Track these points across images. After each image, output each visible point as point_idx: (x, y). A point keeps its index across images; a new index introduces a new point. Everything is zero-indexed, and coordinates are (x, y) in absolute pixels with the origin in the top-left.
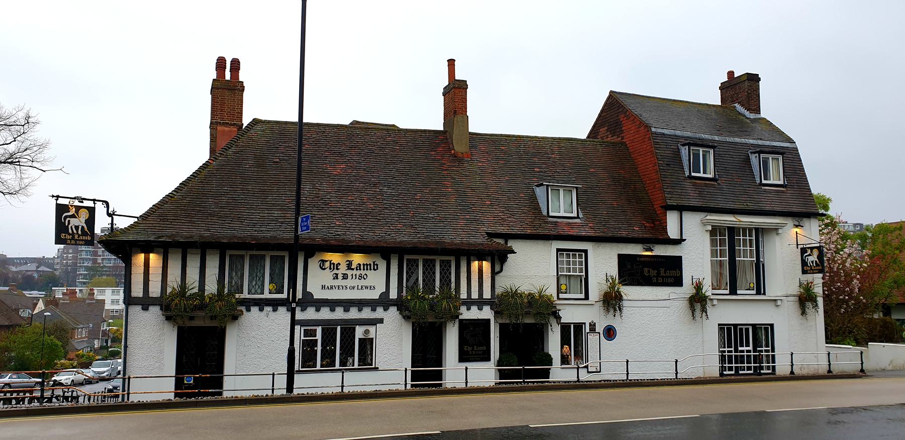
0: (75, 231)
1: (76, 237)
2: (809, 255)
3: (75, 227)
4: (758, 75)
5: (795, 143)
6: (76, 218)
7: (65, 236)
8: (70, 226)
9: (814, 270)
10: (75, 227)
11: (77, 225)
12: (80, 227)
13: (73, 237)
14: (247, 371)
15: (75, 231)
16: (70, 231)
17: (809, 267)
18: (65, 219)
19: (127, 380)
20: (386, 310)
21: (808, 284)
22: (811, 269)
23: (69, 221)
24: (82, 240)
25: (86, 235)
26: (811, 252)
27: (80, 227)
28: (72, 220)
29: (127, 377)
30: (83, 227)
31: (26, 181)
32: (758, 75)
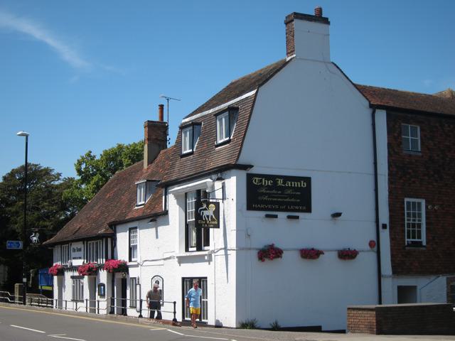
1: (208, 222)
2: (205, 209)
26: (208, 206)
28: (205, 212)
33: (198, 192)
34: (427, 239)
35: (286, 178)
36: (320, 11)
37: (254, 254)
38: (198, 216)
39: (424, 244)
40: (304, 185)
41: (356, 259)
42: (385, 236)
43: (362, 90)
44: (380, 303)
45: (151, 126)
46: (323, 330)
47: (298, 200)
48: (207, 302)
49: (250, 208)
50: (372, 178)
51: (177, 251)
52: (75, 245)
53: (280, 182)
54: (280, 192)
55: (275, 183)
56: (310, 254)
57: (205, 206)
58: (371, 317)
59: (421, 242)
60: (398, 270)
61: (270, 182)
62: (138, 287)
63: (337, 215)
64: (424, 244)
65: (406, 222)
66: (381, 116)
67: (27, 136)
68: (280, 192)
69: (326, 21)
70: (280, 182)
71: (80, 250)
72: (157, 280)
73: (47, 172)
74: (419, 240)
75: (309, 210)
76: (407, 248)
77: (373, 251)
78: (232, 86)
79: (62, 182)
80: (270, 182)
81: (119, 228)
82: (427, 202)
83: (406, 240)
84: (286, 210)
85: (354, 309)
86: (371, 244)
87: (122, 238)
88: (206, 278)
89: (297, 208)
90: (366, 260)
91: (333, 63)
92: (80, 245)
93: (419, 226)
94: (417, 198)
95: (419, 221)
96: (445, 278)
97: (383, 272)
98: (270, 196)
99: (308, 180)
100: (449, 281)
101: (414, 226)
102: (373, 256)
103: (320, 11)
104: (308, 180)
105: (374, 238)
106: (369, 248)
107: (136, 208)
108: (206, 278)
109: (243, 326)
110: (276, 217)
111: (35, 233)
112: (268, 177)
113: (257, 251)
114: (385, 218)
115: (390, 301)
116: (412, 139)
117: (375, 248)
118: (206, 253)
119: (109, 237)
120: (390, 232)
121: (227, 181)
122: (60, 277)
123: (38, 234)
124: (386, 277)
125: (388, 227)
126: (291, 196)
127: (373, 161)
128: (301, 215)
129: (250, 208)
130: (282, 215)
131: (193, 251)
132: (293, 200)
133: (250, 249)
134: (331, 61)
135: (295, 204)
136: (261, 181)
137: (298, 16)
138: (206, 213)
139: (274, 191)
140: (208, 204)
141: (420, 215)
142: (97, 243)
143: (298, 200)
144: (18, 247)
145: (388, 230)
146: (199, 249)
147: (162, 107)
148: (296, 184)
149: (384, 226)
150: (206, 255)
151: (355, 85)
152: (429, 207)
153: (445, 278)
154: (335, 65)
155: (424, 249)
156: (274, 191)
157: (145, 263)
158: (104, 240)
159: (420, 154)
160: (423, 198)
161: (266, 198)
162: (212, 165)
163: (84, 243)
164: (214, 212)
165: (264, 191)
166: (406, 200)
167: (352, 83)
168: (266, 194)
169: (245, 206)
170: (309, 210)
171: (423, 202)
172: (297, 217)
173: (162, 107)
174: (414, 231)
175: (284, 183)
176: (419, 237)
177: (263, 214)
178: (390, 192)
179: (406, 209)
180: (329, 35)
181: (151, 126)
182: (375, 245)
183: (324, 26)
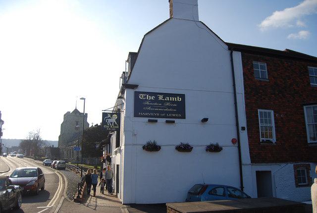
2: (110, 118)
13: (110, 127)
26: (111, 116)
28: (109, 120)
35: (165, 95)
55: (157, 98)
67: (84, 99)
82: (274, 112)
90: (230, 152)
99: (183, 96)
100: (295, 167)
117: (237, 145)
126: (169, 107)
128: (176, 120)
136: (146, 96)
139: (156, 104)
160: (272, 110)
177: (147, 119)
182: (236, 141)
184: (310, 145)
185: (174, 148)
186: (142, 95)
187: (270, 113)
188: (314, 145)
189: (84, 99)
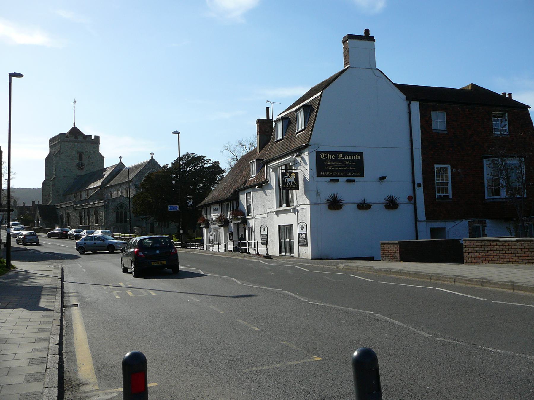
0: (290, 184)
1: (290, 186)
2: (189, 202)
3: (290, 182)
4: (373, 37)
5: (374, 40)
6: (290, 178)
7: (285, 186)
8: (287, 182)
9: (291, 187)
10: (290, 182)
11: (290, 181)
12: (292, 182)
14: (35, 269)
15: (290, 184)
16: (288, 184)
17: (287, 185)
18: (285, 179)
19: (256, 243)
20: (505, 197)
21: (334, 196)
22: (289, 187)
23: (287, 180)
24: (293, 187)
25: (295, 185)
26: (290, 175)
27: (292, 182)
28: (288, 179)
29: (256, 242)
30: (293, 182)
31: (229, 161)
32: (373, 37)
33: (286, 165)
34: (452, 194)
35: (345, 153)
36: (367, 31)
37: (325, 207)
38: (284, 182)
39: (451, 197)
40: (358, 157)
41: (358, 210)
42: (420, 193)
43: (402, 88)
44: (417, 239)
45: (260, 122)
46: (374, 259)
47: (354, 169)
48: (293, 241)
49: (319, 175)
50: (408, 151)
51: (275, 207)
52: (215, 207)
53: (340, 156)
54: (340, 163)
55: (337, 157)
56: (364, 206)
57: (288, 175)
58: (396, 250)
59: (448, 196)
60: (430, 216)
61: (333, 157)
62: (253, 233)
63: (383, 178)
64: (451, 197)
65: (436, 181)
66: (416, 106)
67: (179, 133)
68: (340, 163)
69: (372, 39)
70: (340, 156)
71: (217, 210)
72: (265, 228)
73: (200, 158)
74: (446, 194)
75: (362, 175)
76: (437, 200)
77: (411, 203)
78: (312, 90)
79: (211, 165)
80: (333, 157)
81: (240, 193)
83: (437, 194)
84: (345, 176)
85: (385, 243)
86: (410, 198)
87: (243, 198)
88: (292, 225)
89: (353, 174)
90: (406, 210)
91: (378, 69)
92: (217, 207)
93: (447, 184)
94: (445, 164)
95: (447, 180)
96: (467, 221)
97: (419, 218)
98: (333, 166)
99: (361, 154)
100: (470, 224)
101: (442, 184)
102: (411, 207)
103: (367, 31)
104: (361, 154)
105: (411, 194)
106: (407, 201)
107: (251, 179)
108: (292, 225)
109: (311, 259)
110: (338, 180)
111: (190, 199)
112: (331, 153)
113: (384, 205)
114: (419, 179)
115: (425, 236)
116: (437, 120)
117: (413, 201)
118: (292, 207)
119: (234, 200)
120: (424, 189)
121: (303, 155)
122: (226, 227)
123: (192, 201)
124: (420, 221)
125: (422, 186)
126: (348, 166)
127: (410, 139)
129: (319, 175)
130: (342, 179)
131: (284, 207)
132: (350, 168)
133: (320, 204)
134: (377, 68)
135: (354, 171)
136: (326, 156)
137: (350, 37)
138: (289, 180)
139: (336, 163)
140: (290, 173)
141: (447, 177)
142: (227, 204)
143: (354, 169)
144: (176, 209)
145: (422, 188)
146: (288, 205)
147: (268, 109)
148: (352, 157)
149: (419, 185)
150: (292, 209)
151: (394, 84)
152: (454, 170)
153: (467, 221)
154: (380, 71)
155: (449, 200)
156: (336, 163)
157: (257, 217)
158: (231, 202)
159: (446, 132)
161: (330, 168)
162: (294, 147)
163: (219, 206)
164: (295, 179)
165: (329, 163)
166: (436, 166)
167: (393, 83)
168: (331, 165)
169: (315, 174)
170: (362, 175)
171: (449, 167)
172: (353, 181)
173: (268, 109)
174: (442, 188)
175: (343, 157)
176: (447, 192)
177: (328, 179)
178: (423, 160)
179: (435, 172)
180: (375, 49)
181: (260, 122)
182: (412, 199)
183: (371, 42)
184: (487, 201)
185: (356, 205)
186: (324, 154)
187: (447, 168)
188: (492, 201)
189: (179, 133)
